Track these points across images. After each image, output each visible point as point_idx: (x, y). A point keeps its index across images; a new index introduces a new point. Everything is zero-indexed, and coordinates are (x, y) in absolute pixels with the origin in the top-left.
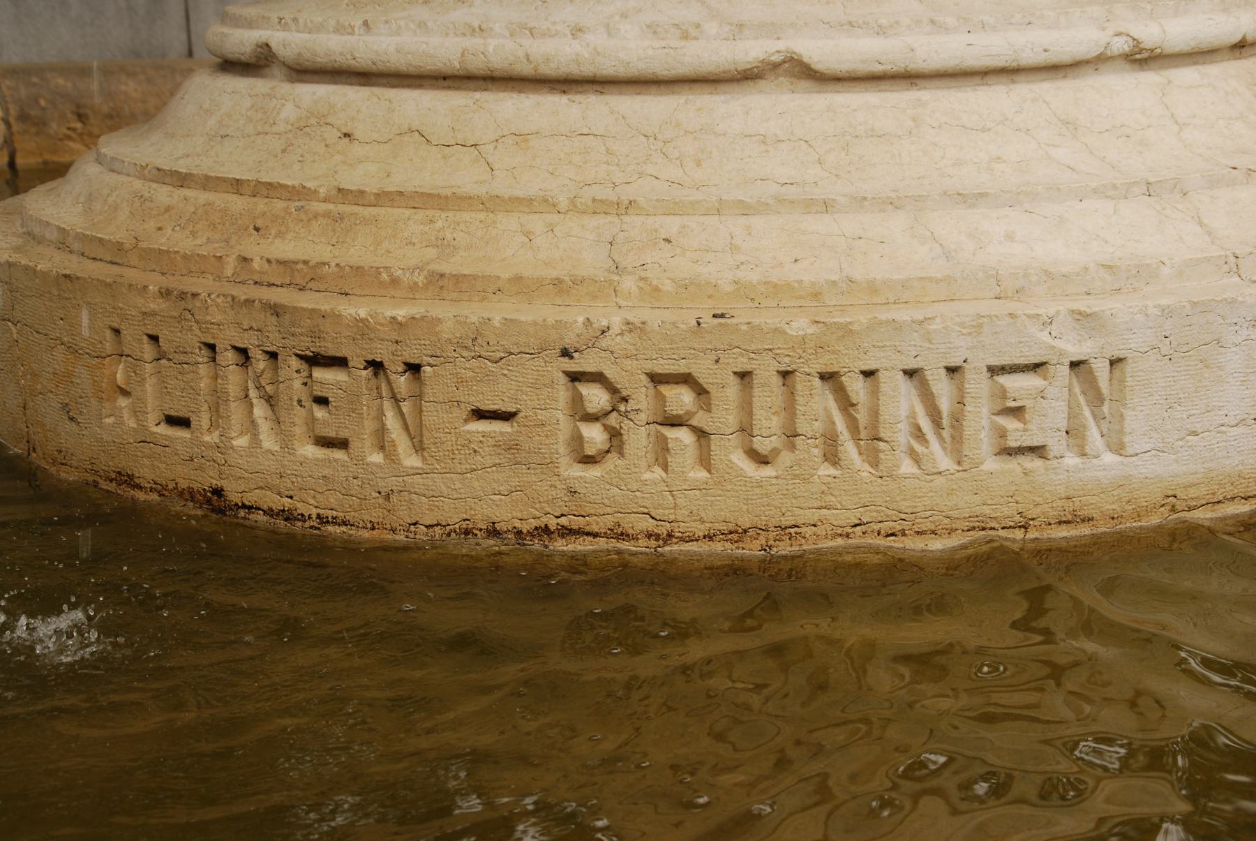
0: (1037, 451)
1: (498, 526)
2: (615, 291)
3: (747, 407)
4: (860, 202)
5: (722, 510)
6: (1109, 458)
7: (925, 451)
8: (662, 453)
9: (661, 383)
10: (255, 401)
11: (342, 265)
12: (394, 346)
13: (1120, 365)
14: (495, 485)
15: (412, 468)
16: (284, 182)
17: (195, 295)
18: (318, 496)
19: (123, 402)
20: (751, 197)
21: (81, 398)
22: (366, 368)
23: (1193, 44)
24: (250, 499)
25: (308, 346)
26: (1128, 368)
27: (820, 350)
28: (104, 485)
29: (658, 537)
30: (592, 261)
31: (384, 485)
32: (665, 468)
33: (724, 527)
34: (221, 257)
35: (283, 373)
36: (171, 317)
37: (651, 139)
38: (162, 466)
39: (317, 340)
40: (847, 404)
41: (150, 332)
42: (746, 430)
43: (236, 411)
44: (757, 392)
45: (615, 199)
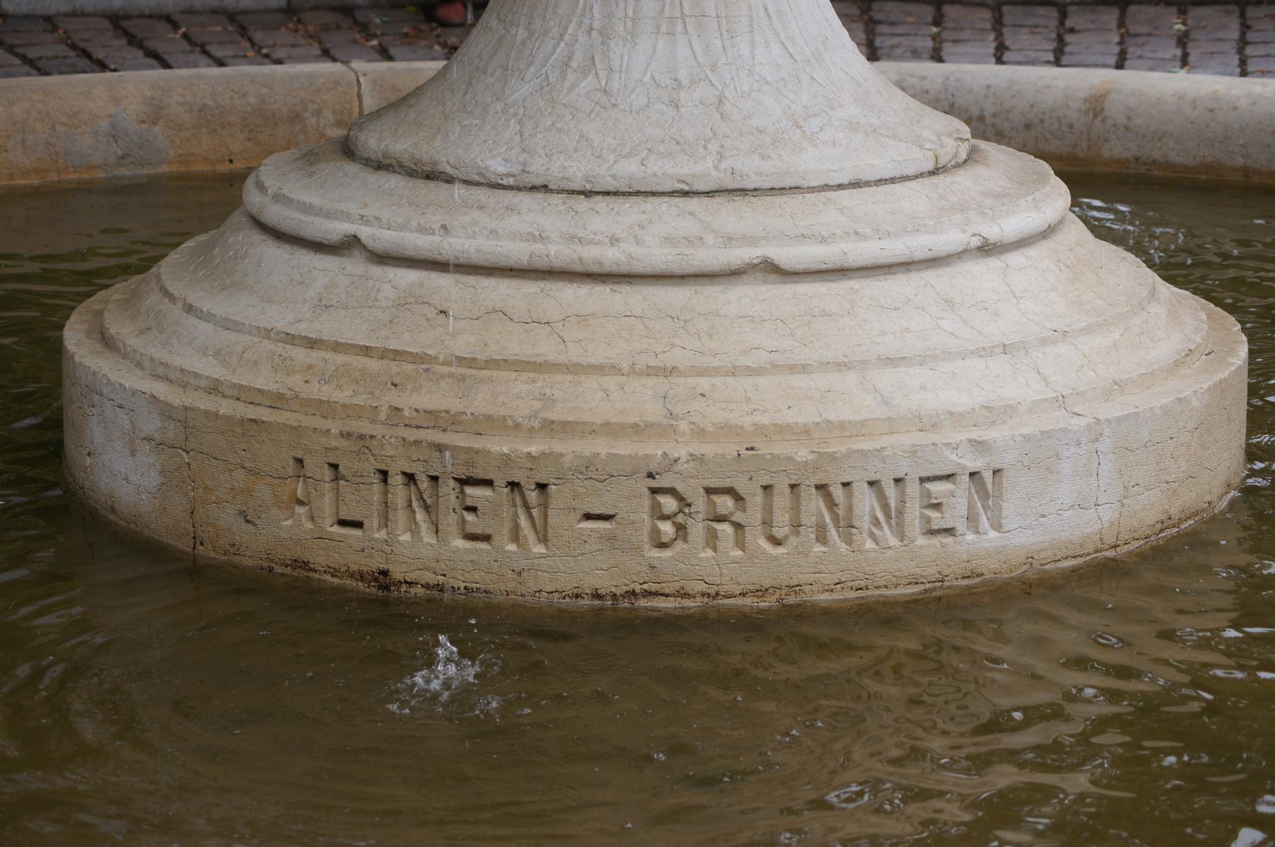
0: (949, 531)
1: (599, 592)
2: (674, 431)
3: (768, 508)
4: (824, 366)
5: (752, 576)
6: (993, 534)
7: (881, 533)
8: (712, 540)
9: (712, 493)
10: (417, 509)
11: (476, 414)
12: (529, 473)
13: (999, 474)
14: (599, 564)
15: (539, 553)
16: (409, 350)
17: (372, 437)
18: (466, 574)
19: (300, 510)
20: (754, 363)
21: (261, 506)
22: (506, 487)
23: (1020, 236)
24: (411, 577)
25: (462, 472)
26: (1005, 474)
27: (816, 470)
28: (278, 569)
29: (709, 595)
30: (654, 412)
31: (515, 566)
32: (715, 549)
33: (753, 588)
34: (376, 407)
35: (442, 491)
36: (351, 452)
37: (676, 319)
38: (336, 556)
39: (471, 468)
40: (832, 504)
41: (330, 461)
42: (767, 523)
43: (401, 516)
44: (775, 498)
45: (662, 365)
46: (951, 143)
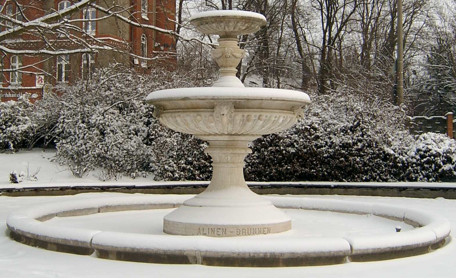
46: (341, 3)
